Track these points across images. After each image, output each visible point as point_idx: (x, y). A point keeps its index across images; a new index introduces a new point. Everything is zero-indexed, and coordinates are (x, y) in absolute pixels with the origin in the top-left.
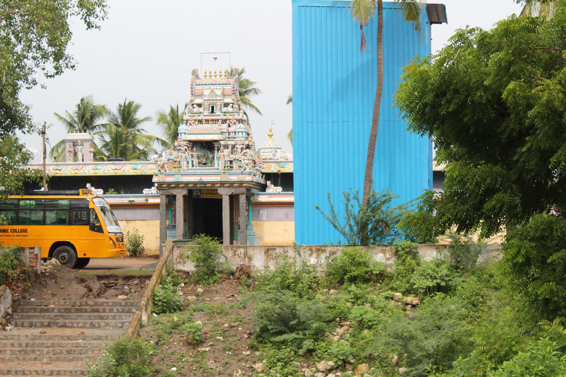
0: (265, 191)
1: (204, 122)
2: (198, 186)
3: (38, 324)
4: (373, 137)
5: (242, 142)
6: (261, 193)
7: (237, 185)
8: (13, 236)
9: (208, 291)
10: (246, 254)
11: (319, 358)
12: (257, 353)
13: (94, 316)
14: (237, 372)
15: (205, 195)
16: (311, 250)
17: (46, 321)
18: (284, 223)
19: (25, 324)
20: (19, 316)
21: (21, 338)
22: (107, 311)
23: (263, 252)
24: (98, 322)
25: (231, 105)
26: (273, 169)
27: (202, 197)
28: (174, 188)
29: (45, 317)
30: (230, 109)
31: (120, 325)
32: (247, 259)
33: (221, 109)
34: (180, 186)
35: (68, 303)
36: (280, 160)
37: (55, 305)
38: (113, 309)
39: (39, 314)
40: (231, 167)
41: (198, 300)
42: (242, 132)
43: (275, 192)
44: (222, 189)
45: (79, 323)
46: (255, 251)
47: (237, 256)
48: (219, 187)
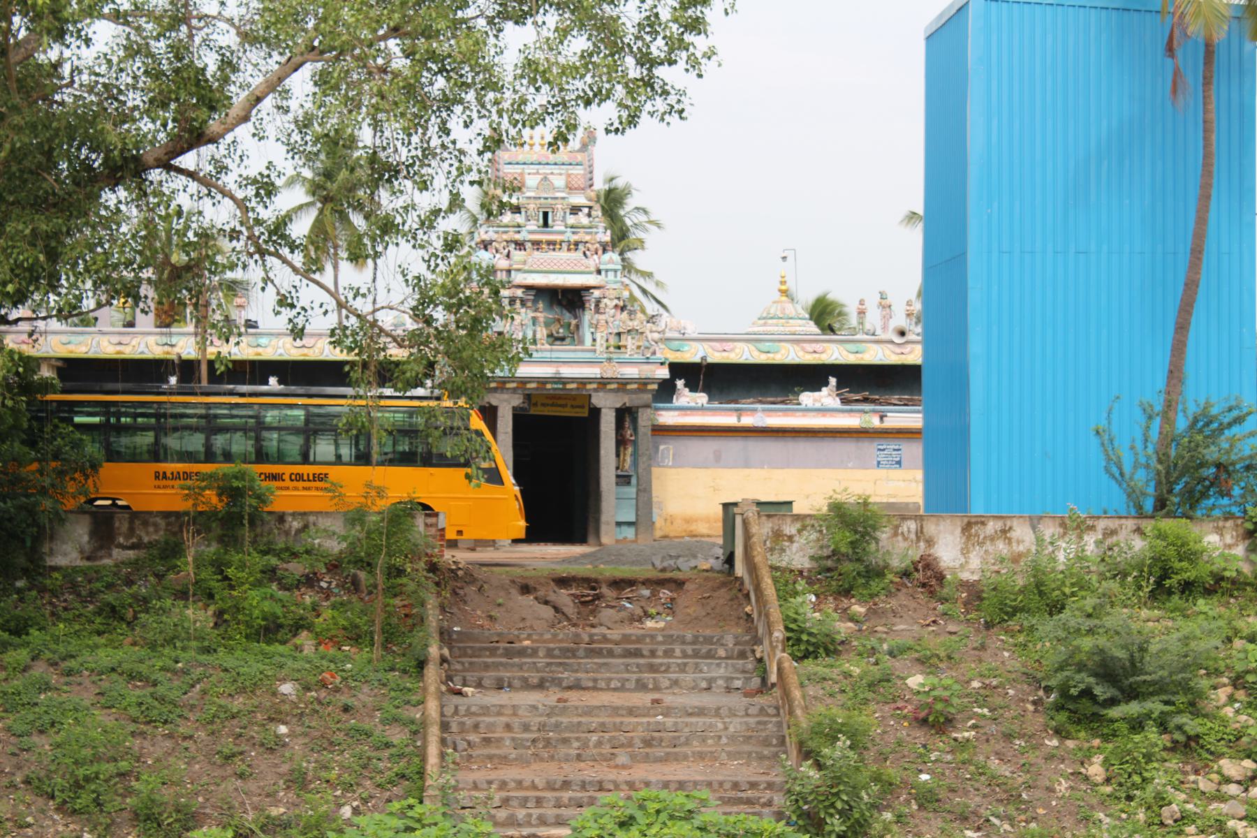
0: (671, 401)
1: (528, 245)
2: (549, 386)
3: (516, 683)
4: (1191, 286)
5: (615, 294)
6: (661, 405)
7: (635, 386)
8: (296, 489)
9: (875, 612)
10: (920, 533)
11: (1212, 753)
12: (1070, 744)
13: (638, 666)
14: (1060, 784)
15: (540, 408)
16: (1063, 524)
17: (534, 678)
18: (710, 471)
19: (486, 682)
20: (463, 664)
21: (520, 712)
22: (660, 653)
23: (959, 530)
24: (654, 679)
25: (586, 210)
26: (692, 354)
27: (533, 412)
28: (495, 390)
29: (525, 668)
30: (582, 219)
31: (704, 685)
32: (922, 544)
33: (564, 217)
34: (508, 386)
35: (561, 636)
36: (668, 335)
37: (533, 641)
38: (673, 650)
39: (504, 660)
40: (619, 348)
41: (860, 630)
42: (616, 271)
43: (693, 404)
44: (601, 394)
45: (611, 679)
46: (941, 527)
47: (900, 538)
48: (596, 390)
